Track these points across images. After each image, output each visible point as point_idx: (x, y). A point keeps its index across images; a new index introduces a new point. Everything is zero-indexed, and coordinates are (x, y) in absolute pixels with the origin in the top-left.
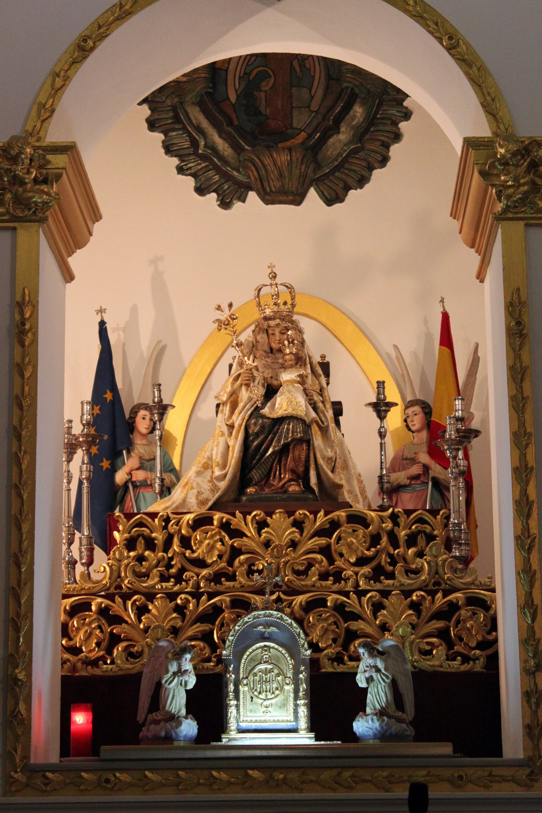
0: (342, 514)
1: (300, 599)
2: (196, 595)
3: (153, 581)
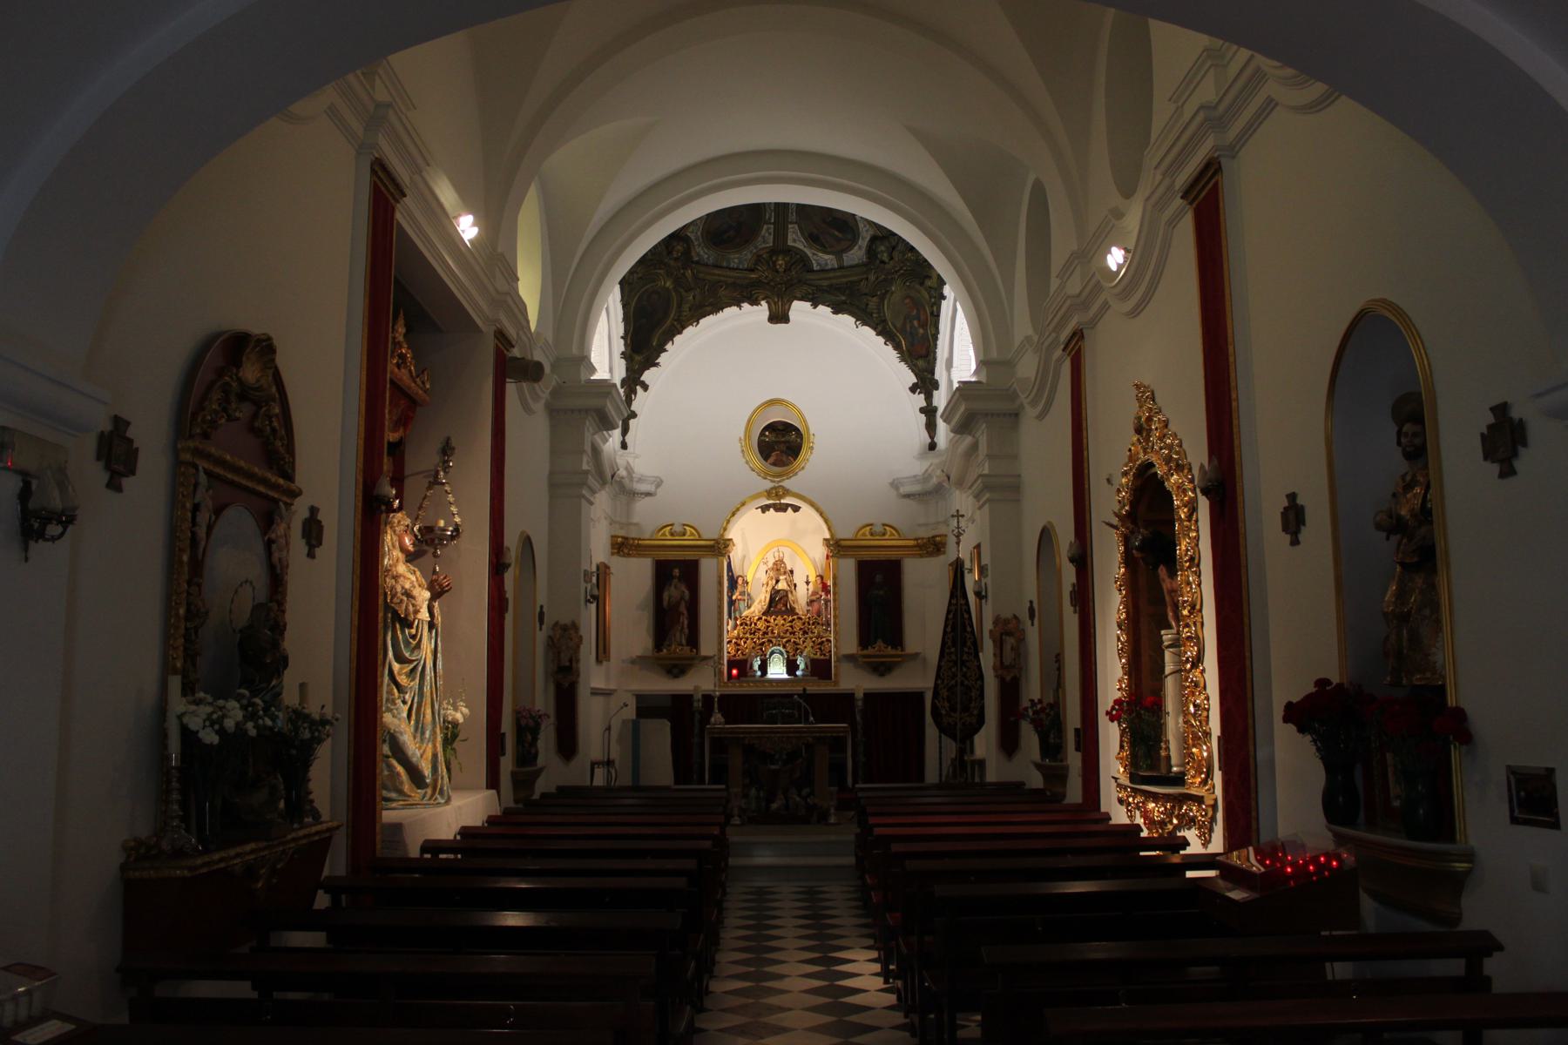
0: (795, 617)
1: (785, 640)
2: (759, 639)
3: (748, 635)
